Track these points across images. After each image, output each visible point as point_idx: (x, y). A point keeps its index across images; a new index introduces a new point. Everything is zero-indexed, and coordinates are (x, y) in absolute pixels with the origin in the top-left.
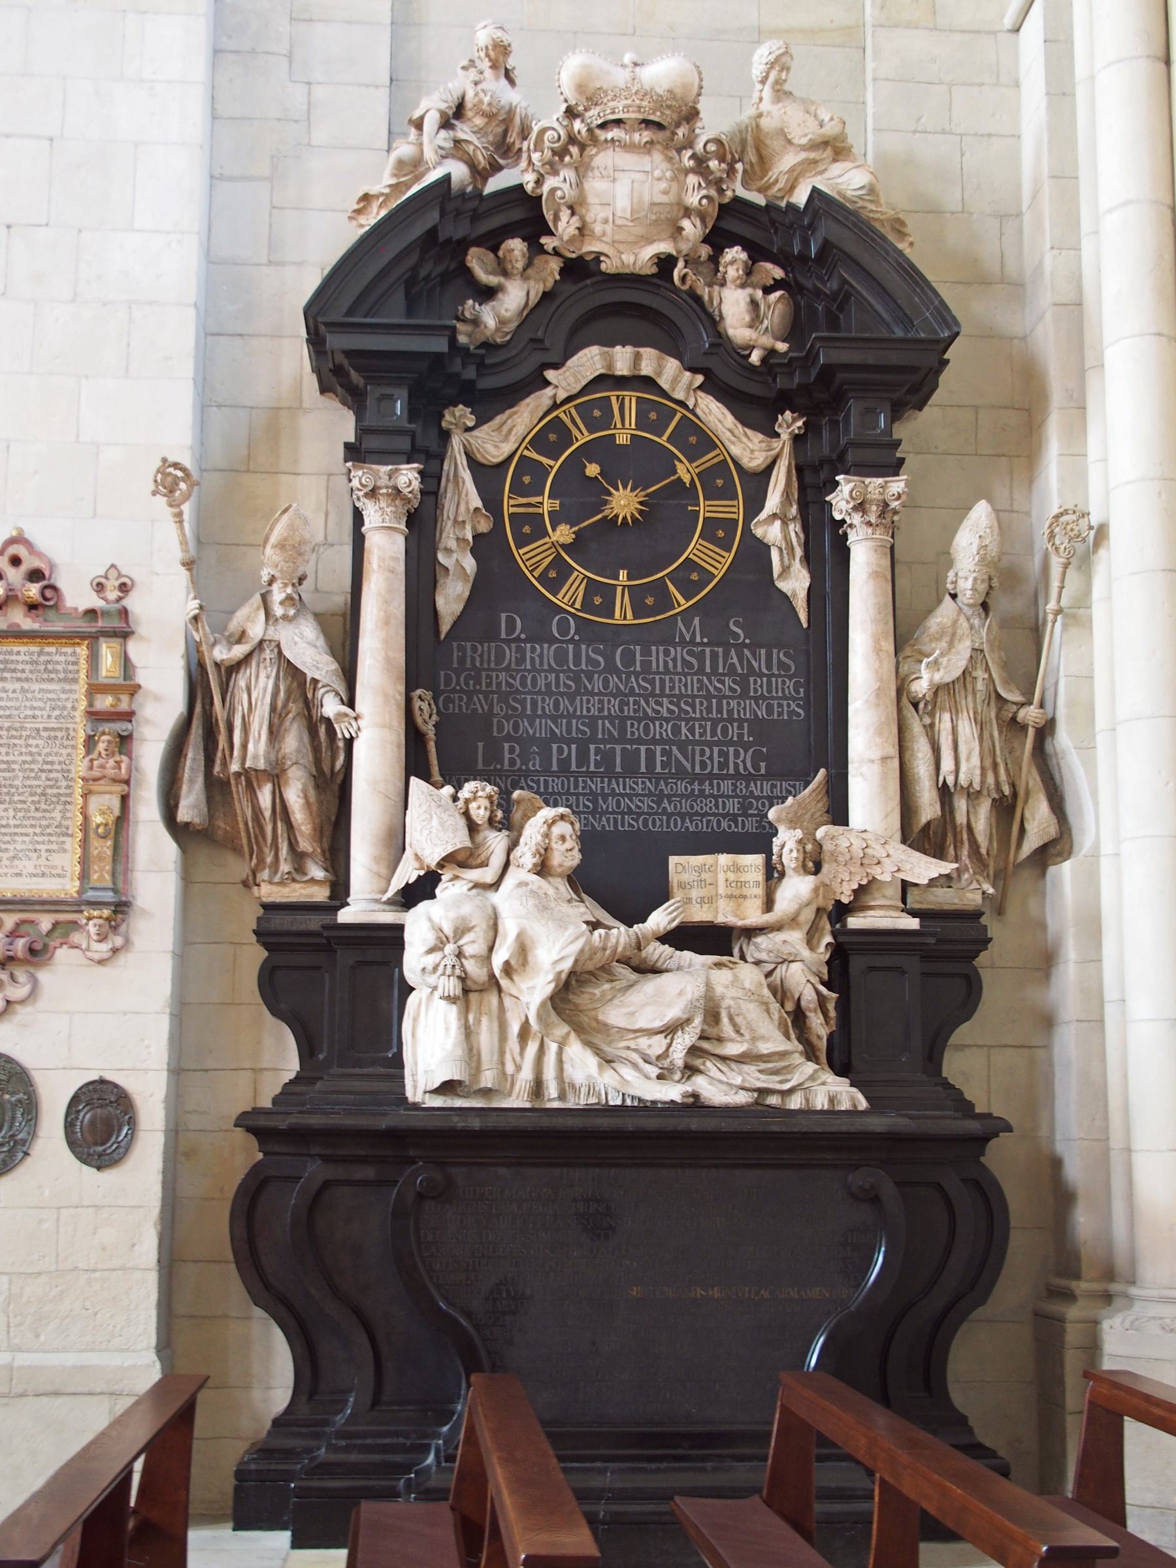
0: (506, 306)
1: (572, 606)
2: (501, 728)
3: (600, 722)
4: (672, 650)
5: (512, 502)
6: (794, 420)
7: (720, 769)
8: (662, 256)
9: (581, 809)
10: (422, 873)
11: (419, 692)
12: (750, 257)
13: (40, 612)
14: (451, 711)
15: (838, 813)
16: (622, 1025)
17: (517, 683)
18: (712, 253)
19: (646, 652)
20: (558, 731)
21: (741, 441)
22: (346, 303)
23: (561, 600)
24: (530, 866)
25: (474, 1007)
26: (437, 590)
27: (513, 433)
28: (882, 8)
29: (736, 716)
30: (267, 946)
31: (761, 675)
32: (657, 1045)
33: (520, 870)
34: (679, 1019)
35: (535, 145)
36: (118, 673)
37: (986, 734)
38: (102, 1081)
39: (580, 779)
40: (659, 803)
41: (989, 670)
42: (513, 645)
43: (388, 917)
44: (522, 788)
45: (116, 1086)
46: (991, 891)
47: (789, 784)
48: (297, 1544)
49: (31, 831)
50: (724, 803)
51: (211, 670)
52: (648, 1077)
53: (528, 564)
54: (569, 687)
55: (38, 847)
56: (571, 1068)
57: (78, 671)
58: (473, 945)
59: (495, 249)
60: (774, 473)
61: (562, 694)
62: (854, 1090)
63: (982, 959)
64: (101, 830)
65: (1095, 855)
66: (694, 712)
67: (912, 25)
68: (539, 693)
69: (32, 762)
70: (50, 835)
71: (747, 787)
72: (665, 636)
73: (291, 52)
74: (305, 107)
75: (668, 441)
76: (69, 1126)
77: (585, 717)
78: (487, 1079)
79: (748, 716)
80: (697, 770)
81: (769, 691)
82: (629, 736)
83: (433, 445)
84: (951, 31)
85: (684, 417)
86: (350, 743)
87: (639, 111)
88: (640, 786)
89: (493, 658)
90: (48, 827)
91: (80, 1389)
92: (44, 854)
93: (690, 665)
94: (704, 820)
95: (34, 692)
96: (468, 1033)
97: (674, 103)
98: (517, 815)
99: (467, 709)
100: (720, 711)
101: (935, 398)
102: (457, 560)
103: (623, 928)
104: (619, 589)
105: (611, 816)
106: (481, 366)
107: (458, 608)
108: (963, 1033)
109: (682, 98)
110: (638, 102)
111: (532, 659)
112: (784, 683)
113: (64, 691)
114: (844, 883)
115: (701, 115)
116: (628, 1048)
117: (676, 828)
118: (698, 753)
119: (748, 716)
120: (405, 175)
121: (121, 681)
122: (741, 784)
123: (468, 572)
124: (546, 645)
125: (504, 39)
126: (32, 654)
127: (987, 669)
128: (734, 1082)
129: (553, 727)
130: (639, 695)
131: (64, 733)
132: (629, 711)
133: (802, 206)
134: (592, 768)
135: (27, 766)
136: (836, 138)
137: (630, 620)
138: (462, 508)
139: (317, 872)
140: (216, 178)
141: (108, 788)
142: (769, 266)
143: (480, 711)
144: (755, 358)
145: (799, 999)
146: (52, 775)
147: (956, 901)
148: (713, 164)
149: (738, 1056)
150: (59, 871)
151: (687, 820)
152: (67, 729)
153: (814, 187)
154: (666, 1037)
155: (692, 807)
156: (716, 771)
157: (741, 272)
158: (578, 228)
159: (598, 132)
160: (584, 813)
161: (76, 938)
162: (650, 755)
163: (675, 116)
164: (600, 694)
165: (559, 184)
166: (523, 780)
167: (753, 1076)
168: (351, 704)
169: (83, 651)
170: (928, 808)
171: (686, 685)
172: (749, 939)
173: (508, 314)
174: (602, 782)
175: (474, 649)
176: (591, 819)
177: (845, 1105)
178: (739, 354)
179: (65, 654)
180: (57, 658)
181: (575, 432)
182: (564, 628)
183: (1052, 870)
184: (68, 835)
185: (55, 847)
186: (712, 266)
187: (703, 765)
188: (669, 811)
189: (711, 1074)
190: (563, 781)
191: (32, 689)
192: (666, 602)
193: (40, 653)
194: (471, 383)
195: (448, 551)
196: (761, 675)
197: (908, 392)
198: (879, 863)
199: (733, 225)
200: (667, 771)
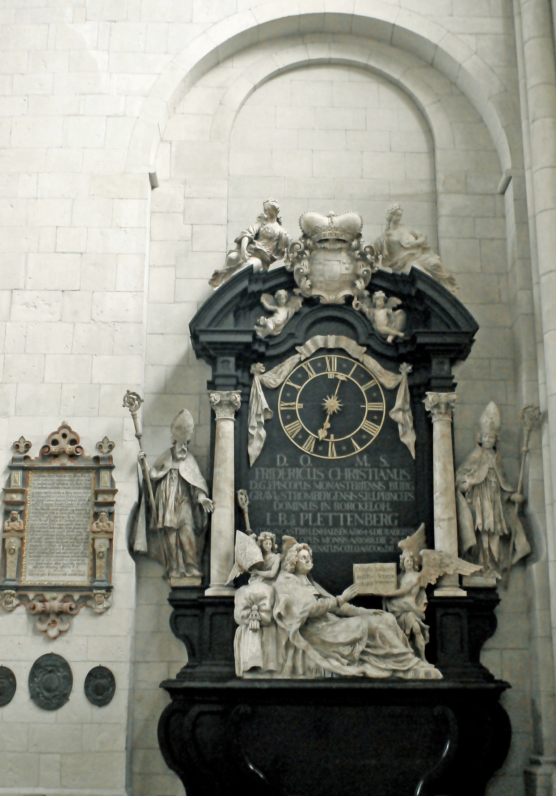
1: (309, 451)
2: (277, 506)
6: (407, 366)
10: (242, 573)
11: (240, 491)
12: (386, 295)
15: (430, 543)
19: (342, 471)
22: (207, 321)
25: (265, 633)
32: (346, 651)
35: (290, 250)
36: (108, 484)
37: (496, 506)
44: (287, 534)
46: (500, 578)
49: (70, 555)
53: (289, 432)
57: (91, 484)
58: (267, 604)
63: (498, 608)
64: (101, 554)
65: (547, 561)
69: (71, 524)
71: (389, 532)
72: (351, 464)
73: (73, 354)
74: (190, 235)
76: (86, 687)
78: (272, 666)
80: (366, 524)
83: (246, 380)
85: (358, 366)
86: (210, 515)
90: (78, 553)
96: (262, 645)
98: (284, 547)
101: (470, 356)
103: (332, 597)
104: (330, 443)
106: (267, 346)
107: (258, 453)
108: (489, 643)
113: (85, 493)
115: (363, 236)
116: (334, 652)
123: (262, 436)
125: (276, 206)
127: (496, 477)
132: (335, 498)
135: (68, 526)
136: (423, 243)
137: (335, 457)
138: (260, 408)
139: (196, 572)
140: (152, 266)
144: (390, 339)
146: (79, 530)
148: (369, 256)
150: (82, 573)
153: (412, 267)
161: (89, 603)
163: (351, 237)
164: (322, 490)
165: (304, 266)
167: (391, 665)
170: (471, 541)
177: (433, 677)
178: (383, 337)
179: (85, 477)
181: (309, 373)
182: (305, 461)
183: (528, 567)
185: (80, 562)
187: (369, 522)
191: (71, 492)
192: (351, 449)
193: (75, 476)
195: (253, 428)
196: (394, 480)
199: (378, 282)
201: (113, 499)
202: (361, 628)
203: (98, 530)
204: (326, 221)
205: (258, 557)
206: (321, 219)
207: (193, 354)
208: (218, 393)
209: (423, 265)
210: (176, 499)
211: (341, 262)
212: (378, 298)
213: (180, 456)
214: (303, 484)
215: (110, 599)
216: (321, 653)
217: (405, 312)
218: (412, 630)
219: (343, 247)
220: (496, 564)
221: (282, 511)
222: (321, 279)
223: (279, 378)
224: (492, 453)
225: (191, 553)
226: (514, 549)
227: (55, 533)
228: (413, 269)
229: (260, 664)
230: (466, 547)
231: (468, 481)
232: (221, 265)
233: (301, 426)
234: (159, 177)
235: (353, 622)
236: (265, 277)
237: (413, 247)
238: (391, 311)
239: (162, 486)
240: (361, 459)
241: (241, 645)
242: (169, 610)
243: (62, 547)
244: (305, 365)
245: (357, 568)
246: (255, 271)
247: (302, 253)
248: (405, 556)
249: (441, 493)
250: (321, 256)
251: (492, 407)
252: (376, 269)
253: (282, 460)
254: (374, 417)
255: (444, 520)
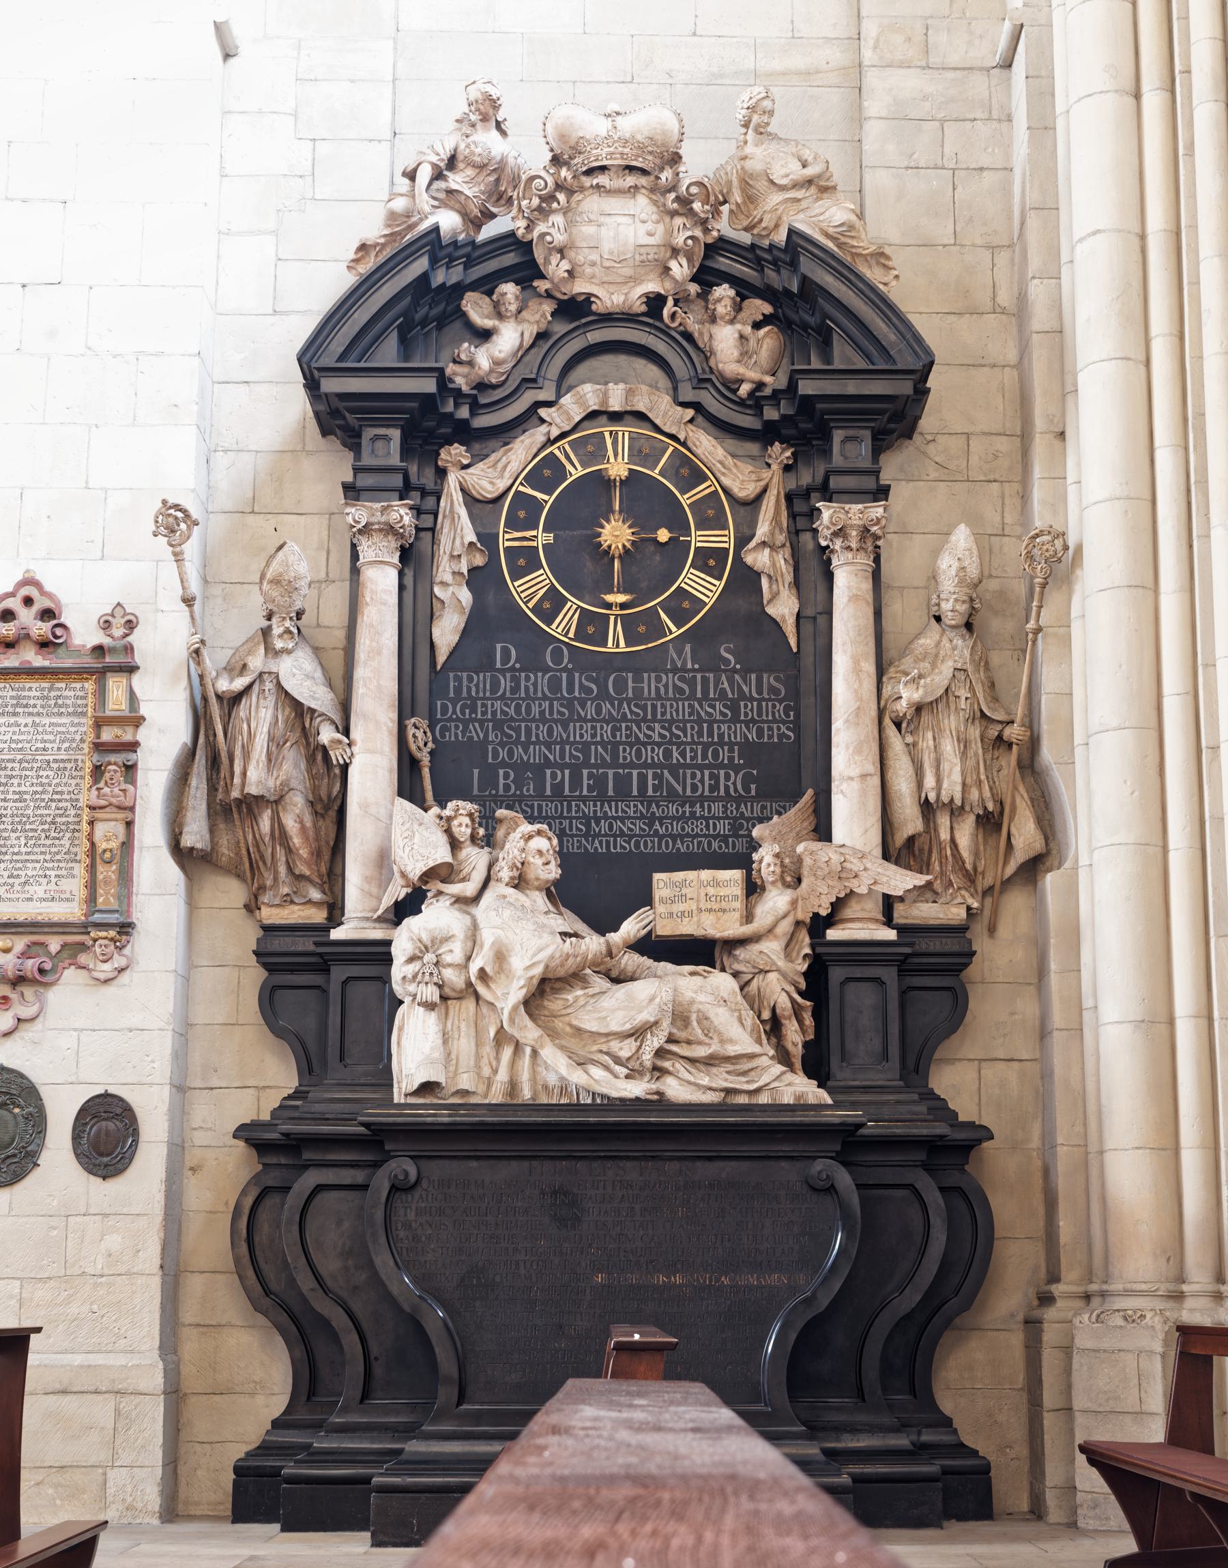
0: (500, 348)
2: (496, 754)
3: (593, 747)
4: (664, 677)
5: (507, 536)
6: (783, 451)
7: (711, 791)
8: (651, 295)
9: (574, 832)
10: (409, 890)
12: (738, 294)
13: (51, 649)
14: (447, 739)
15: (822, 830)
16: (594, 1030)
17: (512, 712)
18: (700, 291)
20: (551, 757)
21: (732, 473)
23: (556, 629)
24: (507, 880)
26: (434, 623)
27: (508, 470)
28: (875, 48)
29: (726, 739)
30: (265, 966)
31: (752, 699)
32: (626, 1049)
33: (499, 884)
34: (647, 1022)
35: (524, 194)
36: (124, 706)
38: (106, 1095)
39: (573, 803)
40: (651, 825)
41: (974, 690)
42: (508, 675)
43: (377, 934)
45: (121, 1099)
47: (779, 806)
48: (283, 1530)
49: (41, 857)
50: (714, 824)
51: (213, 701)
52: (616, 1077)
53: (523, 595)
54: (562, 714)
55: (48, 873)
56: (545, 1072)
57: (86, 705)
58: (454, 952)
59: (490, 293)
60: (765, 502)
61: (556, 721)
62: (821, 1091)
64: (108, 855)
65: (1075, 868)
66: (686, 736)
67: (905, 65)
68: (534, 720)
70: (59, 861)
71: (737, 809)
75: (661, 473)
76: (76, 1137)
77: (578, 743)
79: (739, 739)
80: (688, 792)
81: (760, 715)
82: (621, 761)
83: (428, 480)
84: (943, 69)
86: (345, 768)
87: (622, 158)
88: (632, 809)
89: (488, 687)
90: (58, 853)
91: (85, 1388)
92: (54, 880)
93: (682, 691)
94: (695, 841)
95: (44, 725)
96: (446, 1038)
97: (655, 149)
98: (500, 833)
99: (463, 737)
100: (711, 734)
102: (453, 593)
104: (612, 618)
105: (604, 839)
109: (663, 145)
110: (620, 149)
111: (527, 688)
112: (774, 706)
113: (73, 725)
114: (823, 896)
115: (684, 159)
116: (601, 1051)
117: (667, 849)
118: (689, 776)
119: (739, 739)
120: (398, 225)
121: (127, 713)
122: (732, 806)
123: (464, 604)
124: (540, 674)
125: (492, 93)
126: (43, 689)
127: (972, 689)
128: (701, 1082)
129: (547, 752)
130: (631, 721)
131: (72, 764)
132: (621, 736)
133: (784, 244)
134: (585, 792)
135: (38, 796)
136: (819, 176)
139: (316, 895)
141: (113, 816)
142: (758, 302)
143: (476, 739)
144: (744, 389)
145: (774, 1006)
146: (61, 805)
147: (941, 916)
148: (697, 206)
149: (706, 1057)
151: (679, 842)
152: (76, 760)
154: (636, 1040)
155: (683, 829)
156: (707, 793)
157: (729, 309)
158: (568, 271)
159: (584, 179)
160: (577, 836)
161: (83, 958)
162: (643, 779)
165: (553, 228)
166: (517, 805)
167: (721, 1078)
168: (347, 732)
169: (90, 686)
170: (910, 821)
171: (677, 711)
172: (730, 953)
173: (502, 355)
174: (595, 806)
175: (470, 679)
176: (583, 841)
177: (811, 1100)
179: (74, 689)
180: (67, 693)
181: (569, 467)
184: (76, 861)
185: (64, 872)
186: (703, 304)
187: (694, 788)
188: (661, 832)
189: (680, 1075)
190: (556, 805)
193: (50, 689)
194: (465, 422)
195: (444, 584)
197: (890, 420)
198: (856, 876)
199: (723, 263)
200: (658, 794)
201: (135, 734)
202: (658, 1000)
203: (103, 803)
204: (601, 127)
205: (442, 854)
206: (592, 126)
207: (313, 427)
208: (363, 506)
209: (815, 225)
210: (271, 738)
211: (637, 219)
212: (719, 300)
213: (279, 644)
214: (551, 706)
215: (127, 951)
216: (570, 1054)
217: (781, 330)
218: (774, 1010)
219: (639, 185)
220: (971, 878)
221: (503, 764)
222: (594, 257)
223: (502, 477)
224: (963, 636)
225: (304, 853)
226: (1009, 846)
227: (9, 812)
228: (792, 232)
229: (441, 1078)
230: (900, 838)
231: (907, 695)
232: (374, 230)
233: (548, 581)
234: (240, 33)
235: (641, 989)
236: (472, 253)
237: (795, 185)
238: (748, 330)
239: (242, 710)
240: (680, 653)
241: (404, 1042)
242: (256, 975)
243: (23, 841)
244: (559, 448)
245: (660, 879)
246: (445, 240)
247: (551, 198)
248: (764, 853)
249: (847, 721)
250: (591, 204)
251: (962, 537)
252: (715, 234)
253: (506, 653)
254: (710, 561)
255: (852, 779)
